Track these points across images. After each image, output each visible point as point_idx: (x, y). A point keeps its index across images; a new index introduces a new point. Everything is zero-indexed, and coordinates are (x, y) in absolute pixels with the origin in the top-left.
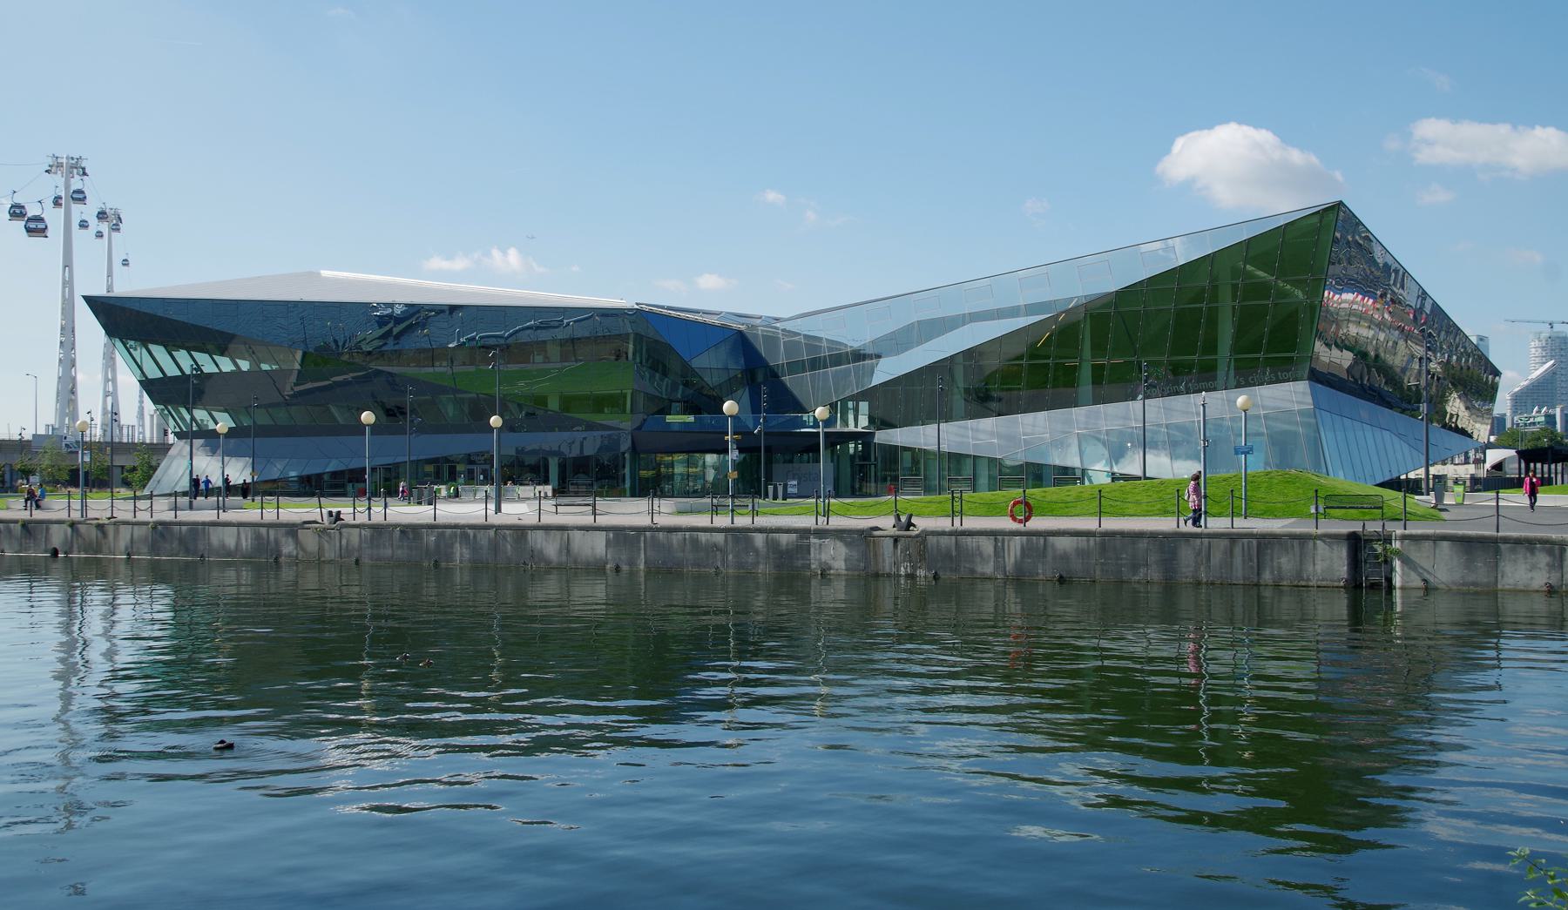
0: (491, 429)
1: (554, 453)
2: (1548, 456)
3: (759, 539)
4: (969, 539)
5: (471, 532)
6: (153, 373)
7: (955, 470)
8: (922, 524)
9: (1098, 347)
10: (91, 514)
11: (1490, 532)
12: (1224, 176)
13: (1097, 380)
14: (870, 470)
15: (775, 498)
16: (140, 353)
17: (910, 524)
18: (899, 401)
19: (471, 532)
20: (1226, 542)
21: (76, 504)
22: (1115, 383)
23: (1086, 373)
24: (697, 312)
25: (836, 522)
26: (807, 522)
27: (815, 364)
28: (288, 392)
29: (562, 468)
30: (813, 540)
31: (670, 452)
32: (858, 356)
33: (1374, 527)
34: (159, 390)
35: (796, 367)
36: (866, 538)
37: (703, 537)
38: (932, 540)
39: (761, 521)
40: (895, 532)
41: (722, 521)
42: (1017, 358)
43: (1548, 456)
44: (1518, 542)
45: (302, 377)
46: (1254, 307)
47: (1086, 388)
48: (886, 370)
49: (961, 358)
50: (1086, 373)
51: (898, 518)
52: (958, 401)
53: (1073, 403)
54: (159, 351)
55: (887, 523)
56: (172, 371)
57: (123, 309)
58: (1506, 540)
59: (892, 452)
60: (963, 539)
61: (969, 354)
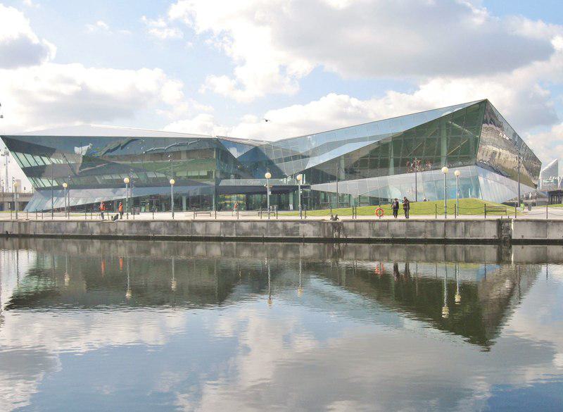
0: (170, 185)
1: (183, 194)
2: (558, 196)
3: (280, 225)
4: (359, 223)
5: (46, 224)
6: (27, 165)
7: (343, 201)
8: (341, 218)
9: (397, 152)
10: (19, 218)
11: (545, 218)
12: (447, 94)
13: (396, 165)
14: (314, 201)
15: (295, 209)
16: (21, 156)
17: (336, 218)
18: (316, 175)
19: (168, 224)
20: (463, 223)
21: (14, 214)
22: (403, 166)
23: (392, 162)
24: (243, 139)
25: (309, 218)
26: (298, 218)
27: (287, 160)
28: (77, 171)
29: (188, 200)
30: (300, 224)
31: (231, 194)
32: (304, 157)
33: (505, 217)
34: (31, 172)
35: (280, 161)
36: (321, 223)
37: (258, 224)
38: (345, 224)
39: (280, 218)
40: (331, 221)
41: (265, 218)
42: (365, 157)
43: (558, 196)
44: (554, 221)
45: (83, 166)
46: (453, 136)
47: (392, 169)
48: (312, 163)
49: (343, 158)
50: (392, 162)
51: (332, 216)
52: (343, 175)
53: (387, 174)
54: (29, 156)
55: (328, 218)
56: (34, 164)
57: (15, 140)
58: (550, 221)
59: (317, 193)
60: (410, 223)
61: (347, 156)
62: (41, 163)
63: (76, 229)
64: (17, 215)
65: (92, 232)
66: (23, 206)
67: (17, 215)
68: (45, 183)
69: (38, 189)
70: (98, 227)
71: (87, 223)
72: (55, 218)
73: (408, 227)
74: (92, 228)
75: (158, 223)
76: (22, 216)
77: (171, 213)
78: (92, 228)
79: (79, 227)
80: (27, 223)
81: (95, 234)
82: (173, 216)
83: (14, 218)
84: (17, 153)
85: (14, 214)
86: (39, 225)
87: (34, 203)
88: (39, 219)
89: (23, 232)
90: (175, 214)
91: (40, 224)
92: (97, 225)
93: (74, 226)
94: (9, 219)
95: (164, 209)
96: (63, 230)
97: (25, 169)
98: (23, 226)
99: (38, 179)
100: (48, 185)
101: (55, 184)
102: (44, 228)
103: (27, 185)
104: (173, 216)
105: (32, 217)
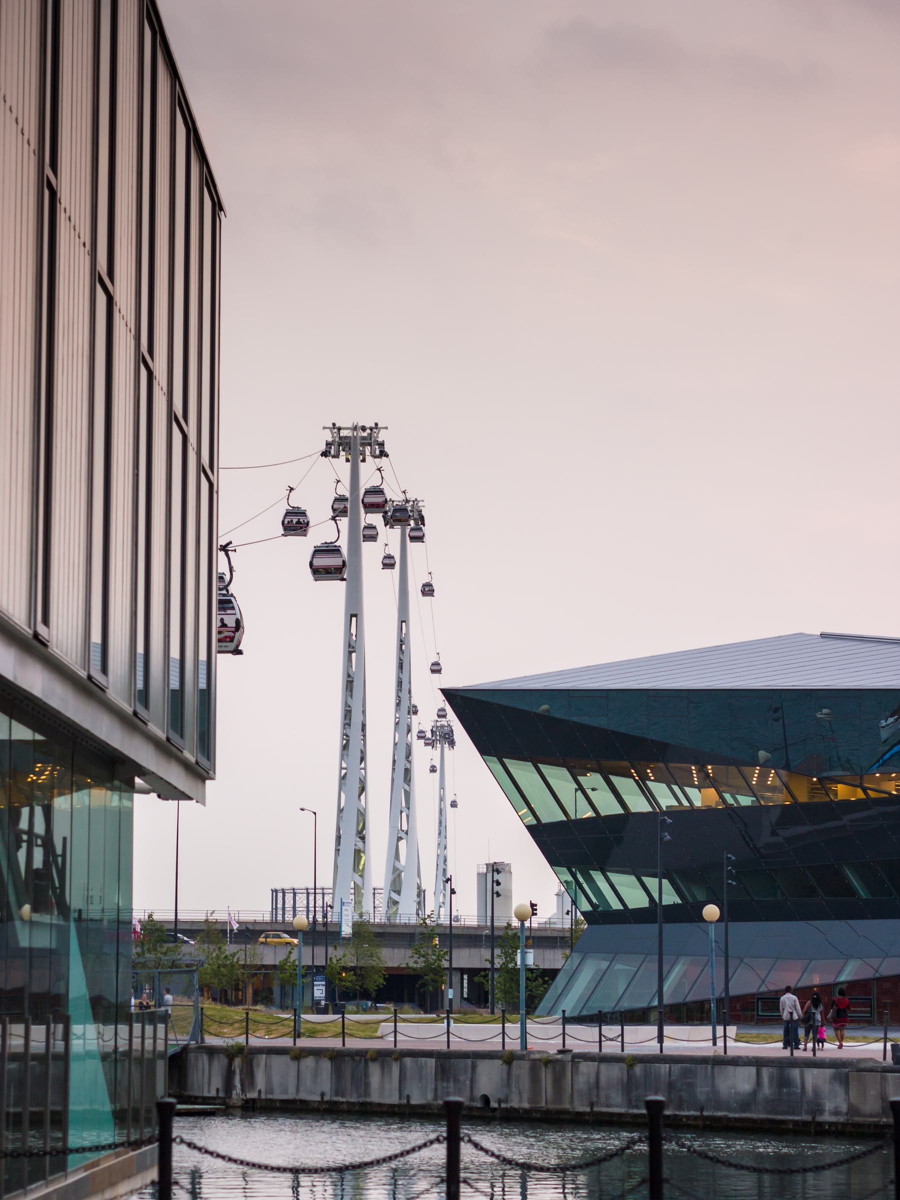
6: (551, 814)
16: (524, 772)
21: (514, 1029)
34: (563, 843)
54: (592, 780)
62: (608, 806)
63: (754, 1093)
64: (524, 1033)
65: (818, 1109)
66: (527, 993)
67: (524, 1033)
68: (630, 891)
69: (600, 916)
70: (839, 1090)
71: (795, 1073)
72: (671, 1046)
73: (783, 1082)
74: (816, 1092)
75: (676, 1068)
76: (544, 1035)
77: (710, 1028)
78: (816, 1092)
79: (767, 1089)
80: (562, 1064)
81: (827, 1117)
82: (661, 1038)
83: (513, 1044)
84: (544, 768)
85: (514, 1029)
86: (613, 1073)
87: (578, 988)
88: (611, 1048)
89: (546, 1100)
90: (668, 1030)
91: (613, 1073)
92: (835, 1078)
93: (741, 1082)
94: (495, 1045)
95: (331, 1011)
96: (701, 1097)
97: (541, 833)
98: (546, 1077)
99: (598, 877)
100: (637, 899)
101: (670, 898)
102: (629, 1086)
103: (540, 892)
104: (661, 1038)
105: (583, 1039)
